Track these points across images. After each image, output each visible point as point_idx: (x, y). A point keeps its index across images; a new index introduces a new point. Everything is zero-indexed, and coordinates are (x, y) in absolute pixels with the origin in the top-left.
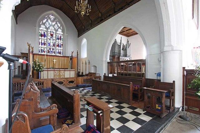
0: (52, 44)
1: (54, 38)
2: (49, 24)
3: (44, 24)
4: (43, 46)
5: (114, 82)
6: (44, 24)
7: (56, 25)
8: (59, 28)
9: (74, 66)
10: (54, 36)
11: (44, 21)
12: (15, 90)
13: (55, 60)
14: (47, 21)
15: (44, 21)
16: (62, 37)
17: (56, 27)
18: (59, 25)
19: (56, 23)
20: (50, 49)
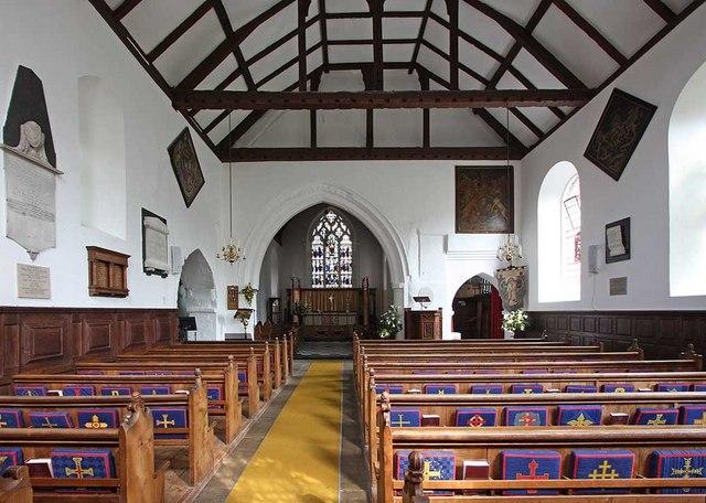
0: (332, 267)
1: (336, 255)
2: (342, 230)
3: (318, 233)
4: (318, 272)
5: (607, 364)
6: (318, 233)
7: (339, 229)
8: (345, 233)
9: (384, 352)
10: (336, 250)
11: (319, 228)
12: (157, 416)
13: (166, 422)
14: (324, 226)
15: (319, 228)
16: (350, 250)
17: (339, 233)
18: (344, 227)
19: (339, 226)
20: (329, 276)
